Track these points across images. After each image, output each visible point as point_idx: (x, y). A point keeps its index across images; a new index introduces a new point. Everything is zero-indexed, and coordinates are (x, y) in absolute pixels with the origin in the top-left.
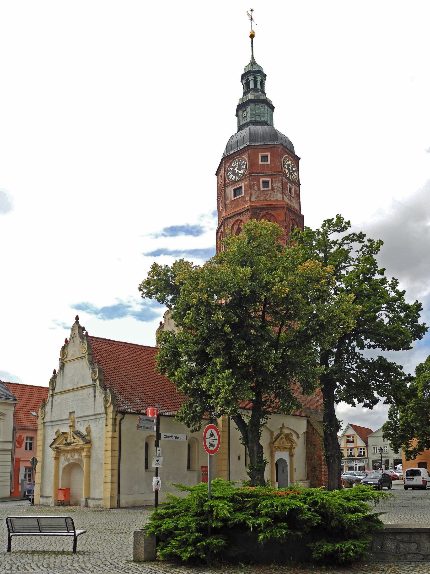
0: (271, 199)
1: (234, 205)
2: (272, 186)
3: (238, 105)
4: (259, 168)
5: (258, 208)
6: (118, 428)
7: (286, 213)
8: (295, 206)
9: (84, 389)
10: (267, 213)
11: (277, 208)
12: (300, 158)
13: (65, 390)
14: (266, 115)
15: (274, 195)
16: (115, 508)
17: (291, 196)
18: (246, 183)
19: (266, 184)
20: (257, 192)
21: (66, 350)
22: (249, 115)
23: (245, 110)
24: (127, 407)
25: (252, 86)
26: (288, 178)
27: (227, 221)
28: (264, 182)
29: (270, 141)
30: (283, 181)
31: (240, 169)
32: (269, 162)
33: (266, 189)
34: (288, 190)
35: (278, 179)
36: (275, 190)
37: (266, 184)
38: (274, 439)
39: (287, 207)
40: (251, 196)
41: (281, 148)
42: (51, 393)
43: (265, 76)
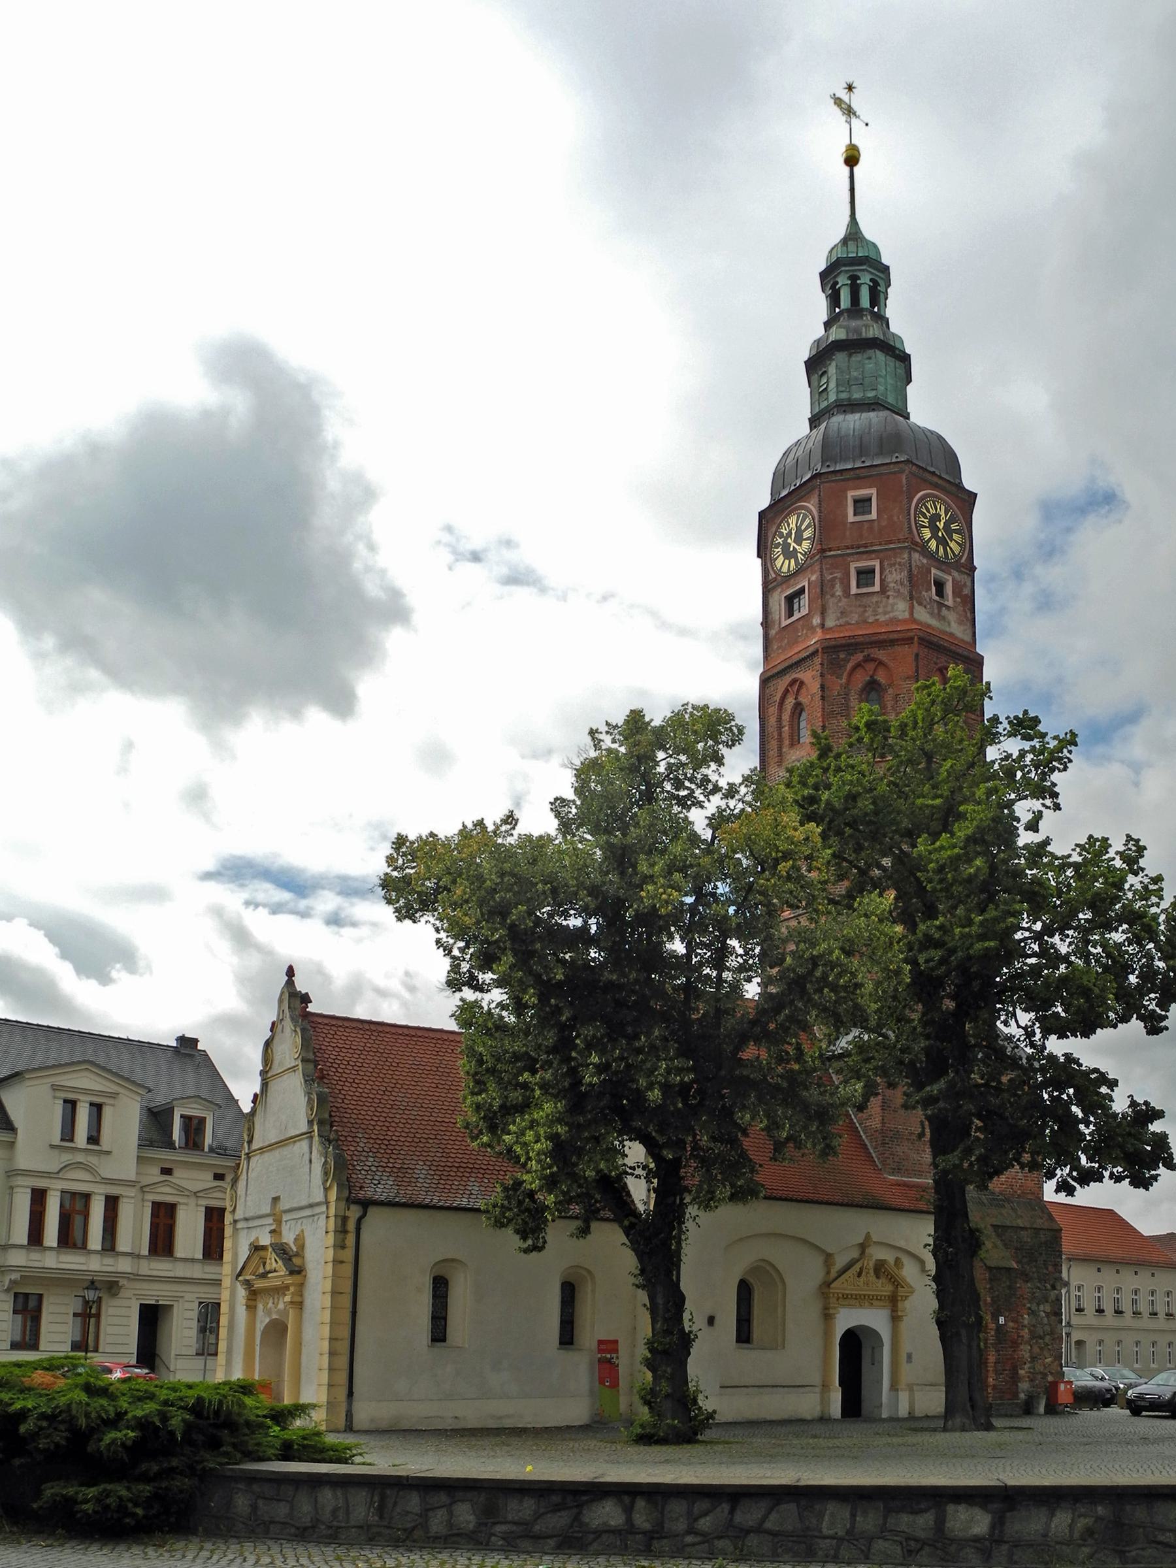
0: (878, 617)
1: (786, 641)
2: (882, 581)
3: (809, 359)
5: (842, 646)
6: (351, 1239)
7: (917, 655)
8: (958, 630)
9: (295, 1142)
10: (868, 659)
11: (893, 642)
12: (976, 495)
13: (267, 1143)
15: (885, 607)
16: (339, 1432)
19: (865, 575)
20: (840, 600)
21: (270, 1051)
22: (832, 385)
23: (825, 372)
24: (382, 1189)
25: (845, 301)
26: (932, 556)
27: (770, 684)
28: (859, 573)
29: (881, 453)
30: (914, 564)
31: (799, 540)
33: (864, 590)
34: (931, 589)
35: (898, 560)
36: (889, 593)
37: (865, 575)
38: (833, 1274)
39: (920, 638)
40: (823, 613)
41: (907, 472)
42: (247, 1151)
43: (886, 269)
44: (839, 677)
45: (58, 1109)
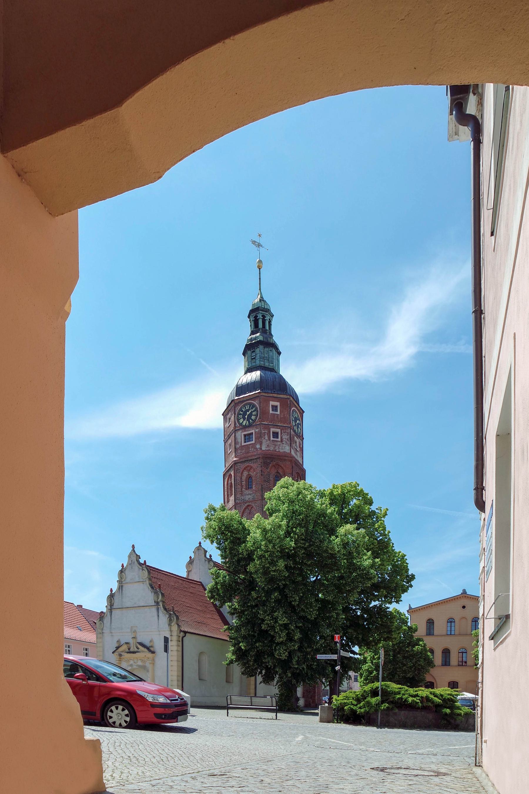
0: (280, 450)
1: (244, 451)
2: (281, 437)
4: (270, 417)
5: (268, 457)
8: (300, 460)
14: (274, 360)
15: (282, 447)
17: (296, 450)
18: (257, 430)
19: (276, 435)
23: (254, 351)
26: (294, 431)
32: (278, 413)
35: (287, 431)
37: (276, 435)
44: (267, 468)
45: (485, 760)
